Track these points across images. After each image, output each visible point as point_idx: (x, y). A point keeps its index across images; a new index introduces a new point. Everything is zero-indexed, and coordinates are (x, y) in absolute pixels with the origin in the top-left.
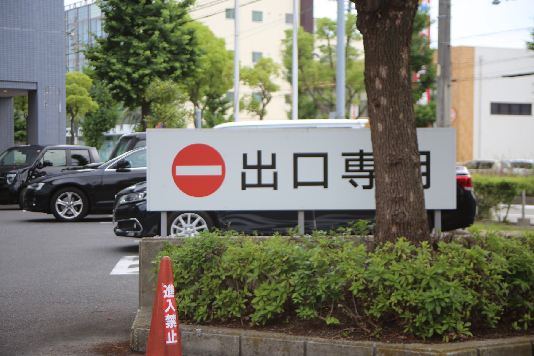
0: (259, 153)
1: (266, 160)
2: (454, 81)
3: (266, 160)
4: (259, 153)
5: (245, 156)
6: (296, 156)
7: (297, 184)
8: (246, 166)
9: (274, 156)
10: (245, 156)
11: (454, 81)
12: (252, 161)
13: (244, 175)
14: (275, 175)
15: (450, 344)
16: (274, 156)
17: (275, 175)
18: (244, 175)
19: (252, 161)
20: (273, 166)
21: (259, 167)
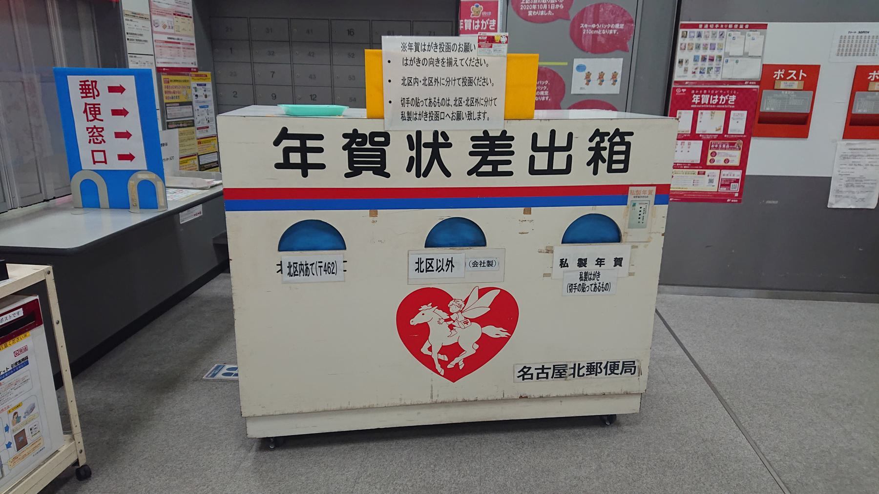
0: (553, 132)
1: (561, 141)
2: (163, 145)
3: (561, 141)
4: (553, 132)
5: (535, 136)
6: (104, 151)
7: (93, 151)
8: (535, 148)
9: (570, 135)
10: (535, 136)
11: (163, 145)
12: (543, 142)
13: (532, 158)
14: (569, 158)
15: (109, 212)
16: (570, 135)
17: (569, 158)
18: (532, 158)
19: (543, 142)
20: (568, 147)
21: (551, 149)
